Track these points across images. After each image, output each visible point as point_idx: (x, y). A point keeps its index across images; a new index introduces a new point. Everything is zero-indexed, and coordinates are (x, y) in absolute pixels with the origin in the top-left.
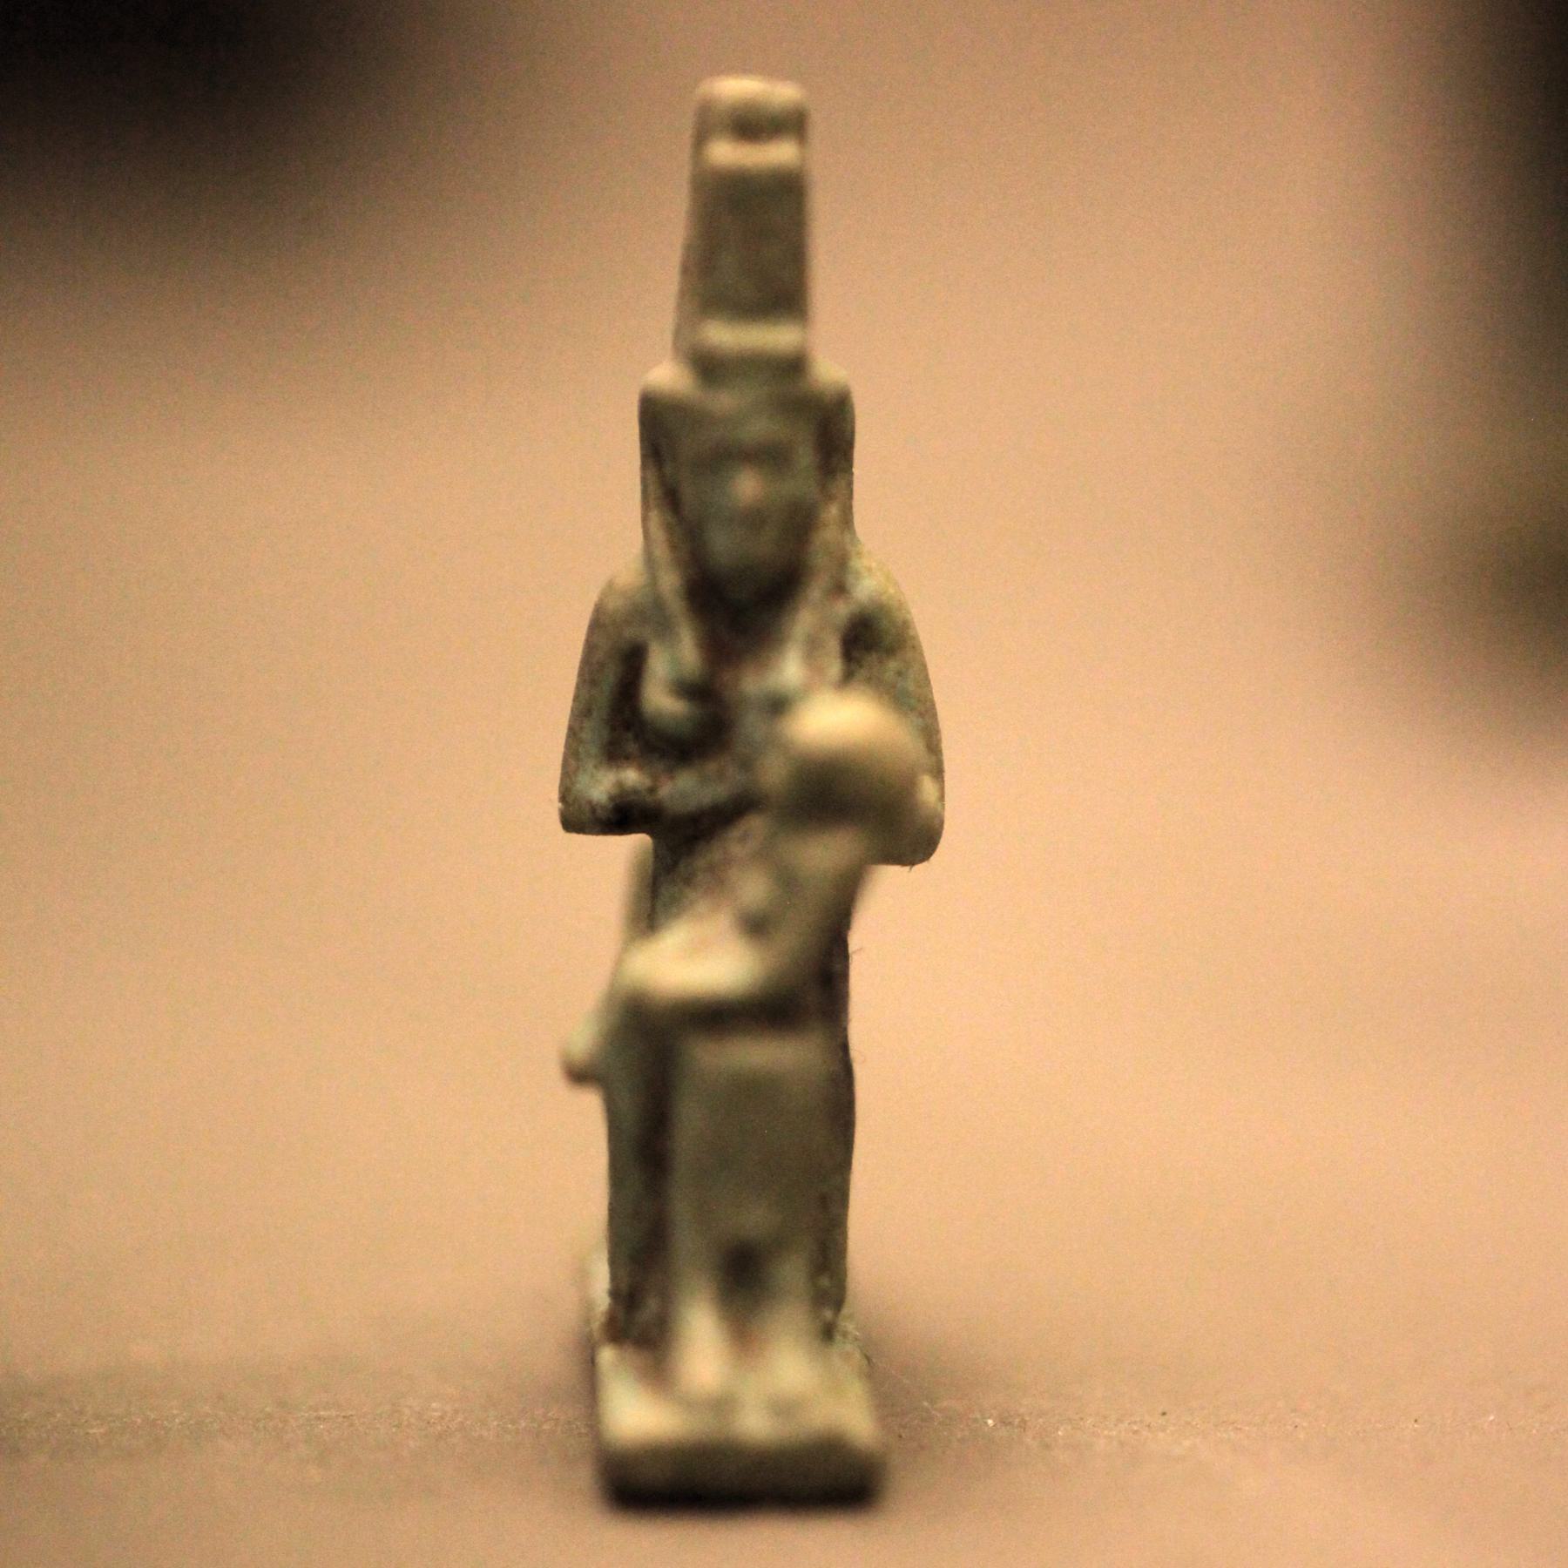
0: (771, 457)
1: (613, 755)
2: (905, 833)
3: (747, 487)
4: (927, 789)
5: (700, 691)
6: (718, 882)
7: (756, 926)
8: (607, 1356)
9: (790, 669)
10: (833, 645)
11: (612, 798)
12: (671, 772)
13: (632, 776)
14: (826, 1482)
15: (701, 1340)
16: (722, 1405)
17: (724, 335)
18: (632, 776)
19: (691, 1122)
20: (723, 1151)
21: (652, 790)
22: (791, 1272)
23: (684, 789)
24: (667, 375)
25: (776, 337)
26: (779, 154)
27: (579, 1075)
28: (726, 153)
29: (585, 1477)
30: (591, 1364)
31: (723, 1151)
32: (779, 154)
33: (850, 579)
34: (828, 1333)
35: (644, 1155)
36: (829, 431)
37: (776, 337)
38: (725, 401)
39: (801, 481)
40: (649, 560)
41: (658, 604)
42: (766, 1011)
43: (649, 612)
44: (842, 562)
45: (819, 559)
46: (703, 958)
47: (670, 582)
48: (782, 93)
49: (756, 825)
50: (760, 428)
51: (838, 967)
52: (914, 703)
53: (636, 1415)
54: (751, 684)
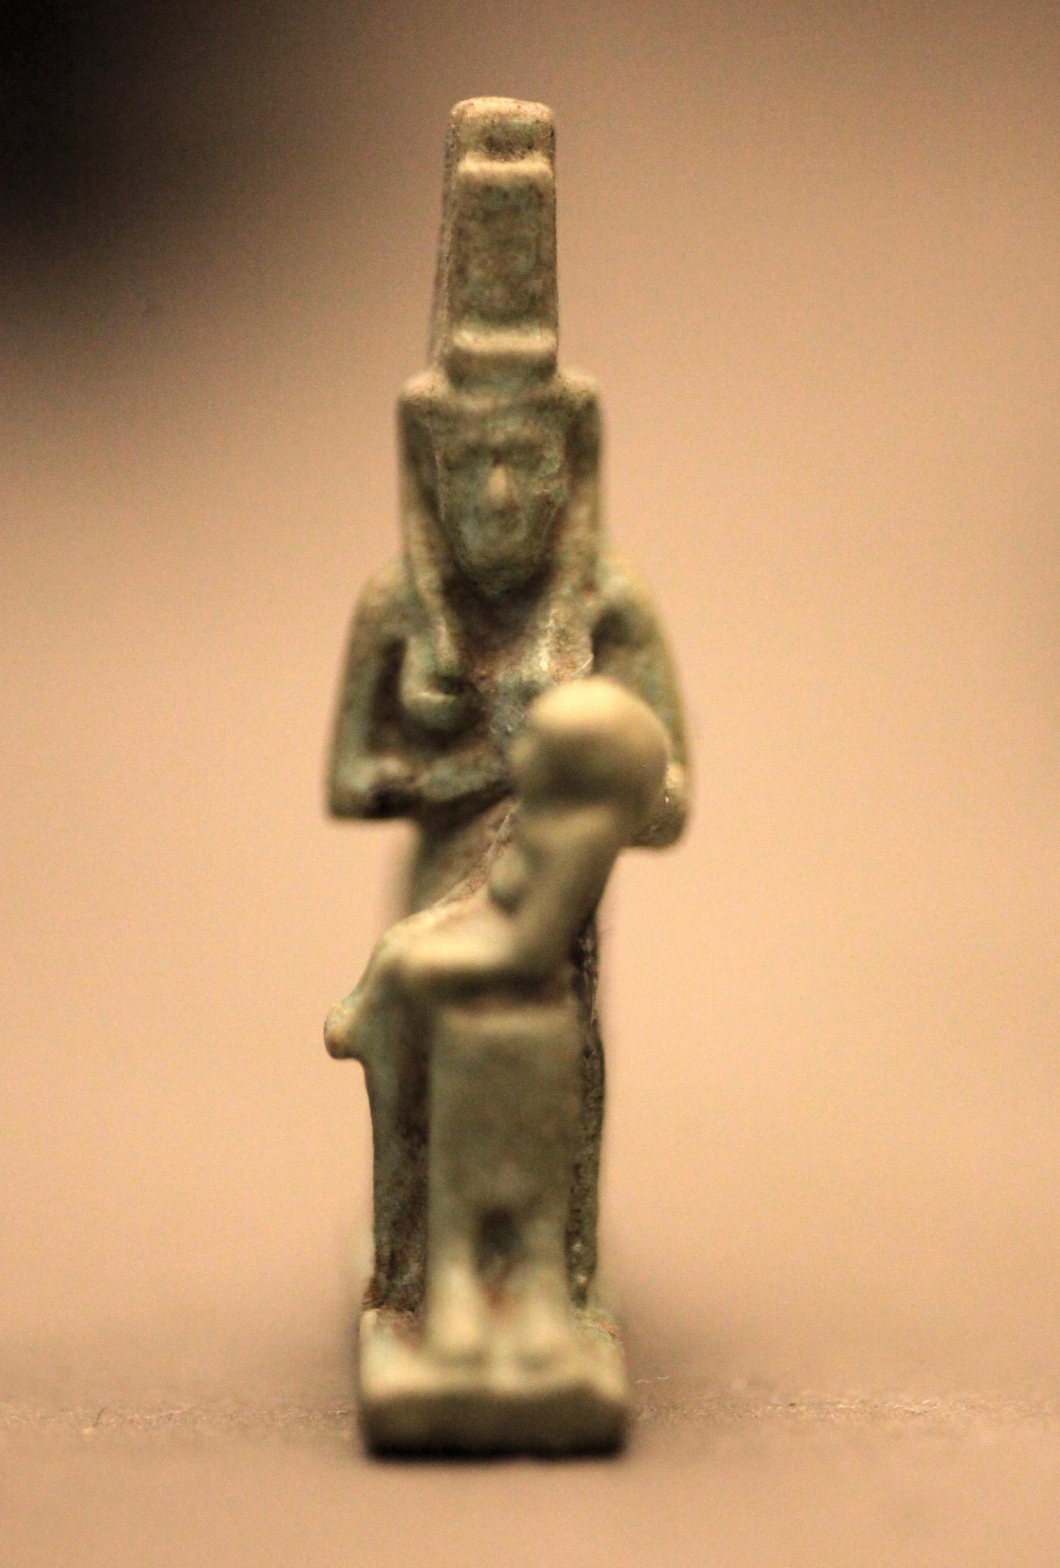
0: (517, 455)
1: (375, 746)
2: (651, 818)
3: (498, 483)
4: (673, 776)
5: (451, 682)
6: (475, 862)
7: (507, 904)
8: (370, 1316)
9: (541, 660)
10: (584, 639)
11: (374, 787)
12: (429, 762)
13: (393, 767)
14: (576, 1434)
15: (457, 1295)
16: (477, 1359)
17: (473, 339)
18: (393, 767)
19: (444, 1086)
20: (480, 1119)
21: (412, 779)
22: (543, 1234)
23: (444, 777)
24: (427, 383)
25: (531, 341)
26: (533, 165)
27: (338, 1050)
28: (474, 165)
29: (348, 1433)
30: (355, 1329)
31: (480, 1119)
32: (533, 165)
33: (598, 576)
34: (580, 1297)
35: (404, 1122)
36: (579, 435)
37: (531, 341)
38: (475, 403)
39: (548, 480)
40: (407, 558)
41: (416, 600)
42: (513, 984)
43: (409, 609)
44: (591, 560)
45: (568, 553)
46: (460, 934)
47: (428, 579)
48: (532, 111)
49: (511, 808)
50: (510, 429)
51: (588, 946)
52: (660, 693)
53: (395, 1370)
54: (504, 675)
